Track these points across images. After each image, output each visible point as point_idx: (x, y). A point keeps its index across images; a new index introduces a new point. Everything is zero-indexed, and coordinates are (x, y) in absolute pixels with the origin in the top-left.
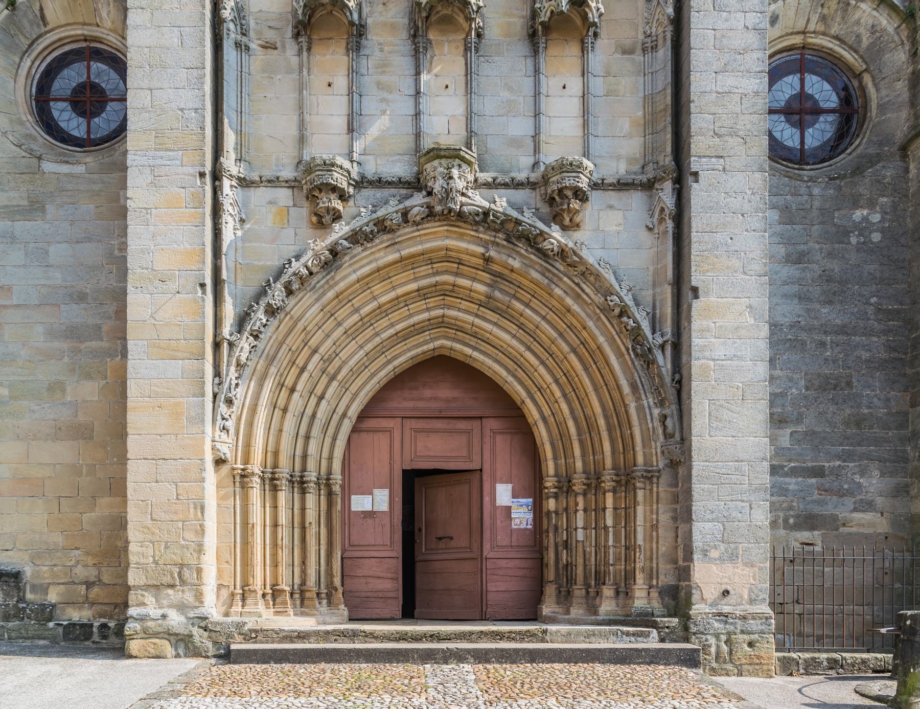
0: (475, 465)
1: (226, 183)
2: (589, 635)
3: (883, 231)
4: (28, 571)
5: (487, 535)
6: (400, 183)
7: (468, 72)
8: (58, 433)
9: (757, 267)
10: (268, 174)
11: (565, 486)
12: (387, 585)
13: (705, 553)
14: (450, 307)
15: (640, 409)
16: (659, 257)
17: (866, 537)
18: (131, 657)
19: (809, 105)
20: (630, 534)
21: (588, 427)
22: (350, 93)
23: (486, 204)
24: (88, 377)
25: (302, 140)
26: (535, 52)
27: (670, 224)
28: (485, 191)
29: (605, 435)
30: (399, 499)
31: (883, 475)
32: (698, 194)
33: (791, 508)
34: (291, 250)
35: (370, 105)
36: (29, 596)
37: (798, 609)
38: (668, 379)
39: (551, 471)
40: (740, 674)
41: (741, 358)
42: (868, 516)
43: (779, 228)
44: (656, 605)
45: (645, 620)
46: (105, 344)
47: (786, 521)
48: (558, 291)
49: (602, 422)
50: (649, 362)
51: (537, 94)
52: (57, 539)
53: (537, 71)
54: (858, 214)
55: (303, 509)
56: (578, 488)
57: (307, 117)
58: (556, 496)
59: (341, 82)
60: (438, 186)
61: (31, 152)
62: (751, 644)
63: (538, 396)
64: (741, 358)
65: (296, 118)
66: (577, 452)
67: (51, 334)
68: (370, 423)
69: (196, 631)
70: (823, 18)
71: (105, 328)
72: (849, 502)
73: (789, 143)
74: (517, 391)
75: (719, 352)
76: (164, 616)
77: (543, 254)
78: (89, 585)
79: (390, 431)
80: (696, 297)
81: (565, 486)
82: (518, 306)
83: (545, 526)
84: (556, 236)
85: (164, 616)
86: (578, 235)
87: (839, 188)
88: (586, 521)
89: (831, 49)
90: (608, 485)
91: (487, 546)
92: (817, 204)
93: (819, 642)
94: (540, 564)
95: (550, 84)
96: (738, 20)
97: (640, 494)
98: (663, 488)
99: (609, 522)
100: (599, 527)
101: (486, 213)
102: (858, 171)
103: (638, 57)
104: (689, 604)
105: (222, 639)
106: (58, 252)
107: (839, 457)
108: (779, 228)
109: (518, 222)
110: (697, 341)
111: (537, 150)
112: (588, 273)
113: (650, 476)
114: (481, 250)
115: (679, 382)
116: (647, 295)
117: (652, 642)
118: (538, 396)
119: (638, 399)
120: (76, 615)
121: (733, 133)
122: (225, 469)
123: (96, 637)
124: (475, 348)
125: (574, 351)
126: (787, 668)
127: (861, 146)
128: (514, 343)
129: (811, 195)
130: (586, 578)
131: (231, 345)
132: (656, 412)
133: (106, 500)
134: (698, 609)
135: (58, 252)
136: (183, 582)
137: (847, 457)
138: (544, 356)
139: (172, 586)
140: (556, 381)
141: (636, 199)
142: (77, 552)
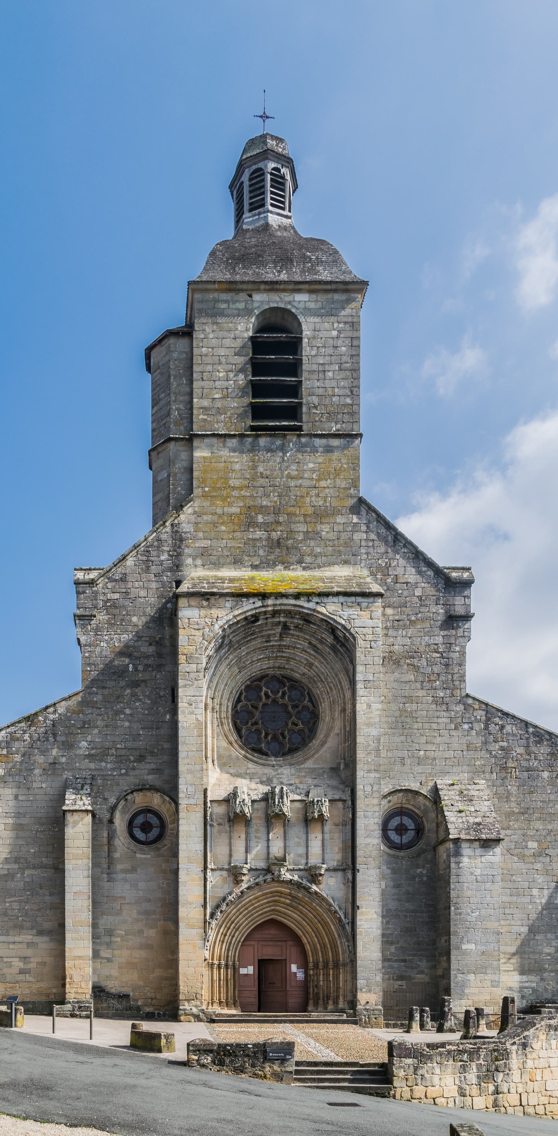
0: (284, 958)
1: (208, 871)
2: (324, 1016)
3: (427, 877)
4: (131, 994)
5: (288, 982)
6: (263, 869)
7: (285, 833)
8: (142, 947)
9: (378, 899)
10: (220, 867)
11: (316, 966)
12: (253, 1000)
13: (361, 990)
14: (277, 906)
15: (341, 942)
16: (347, 894)
17: (421, 983)
18: (181, 1021)
19: (404, 828)
20: (338, 983)
21: (324, 947)
22: (246, 840)
23: (291, 877)
24: (152, 928)
25: (230, 855)
26: (307, 826)
27: (350, 884)
28: (290, 872)
29: (330, 950)
30: (257, 970)
31: (427, 961)
32: (359, 876)
33: (395, 973)
34: (227, 891)
35: (252, 844)
36: (132, 1003)
37: (398, 1008)
38: (350, 934)
39: (311, 961)
40: (372, 1028)
41: (372, 928)
42: (422, 976)
43: (391, 876)
44: (346, 1006)
45: (342, 1011)
46: (157, 916)
47: (393, 978)
48: (314, 904)
49: (329, 946)
50: (344, 928)
51: (307, 840)
52: (141, 983)
53: (307, 833)
54: (419, 871)
55: (227, 974)
56: (321, 967)
57: (233, 848)
58: (313, 969)
59: (243, 836)
60: (276, 873)
61: (132, 850)
62: (375, 1018)
63: (307, 935)
64: (372, 928)
65: (228, 848)
66: (320, 955)
67: (139, 913)
68: (246, 943)
69: (201, 1014)
70: (407, 800)
71: (157, 911)
72: (415, 971)
73: (397, 841)
74: (300, 933)
75: (366, 927)
76: (191, 1009)
77: (310, 893)
78: (152, 999)
79: (254, 946)
80: (358, 909)
81: (316, 966)
82: (300, 907)
83: (309, 979)
84: (314, 888)
85: (191, 1009)
86: (321, 886)
87: (412, 862)
88: (324, 978)
89: (411, 810)
90: (331, 967)
91: (288, 986)
92: (404, 867)
93: (398, 1018)
94: (307, 993)
95: (312, 836)
96: (372, 821)
97: (341, 970)
98: (349, 968)
99: (331, 979)
100: (328, 981)
101: (291, 880)
102: (419, 855)
103: (341, 827)
104: (356, 1006)
105: (209, 1017)
106: (141, 885)
107: (412, 955)
108: (391, 876)
109: (302, 884)
110: (358, 923)
111: (307, 858)
112: (324, 899)
113: (344, 965)
114: (289, 891)
115: (354, 935)
116: (343, 906)
117: (345, 1017)
118: (307, 935)
119: (340, 939)
120: (148, 1009)
121: (370, 857)
122: (206, 962)
123: (156, 1017)
124: (285, 918)
125: (319, 922)
126: (387, 1026)
127: (421, 845)
128: (299, 918)
129: (402, 864)
130: (323, 997)
131: (209, 923)
132: (346, 944)
133: (158, 970)
134: (359, 1007)
135: (141, 885)
136: (197, 999)
137: (415, 955)
138: (309, 922)
139: (193, 1000)
140: (313, 931)
141: (340, 874)
142: (148, 988)
